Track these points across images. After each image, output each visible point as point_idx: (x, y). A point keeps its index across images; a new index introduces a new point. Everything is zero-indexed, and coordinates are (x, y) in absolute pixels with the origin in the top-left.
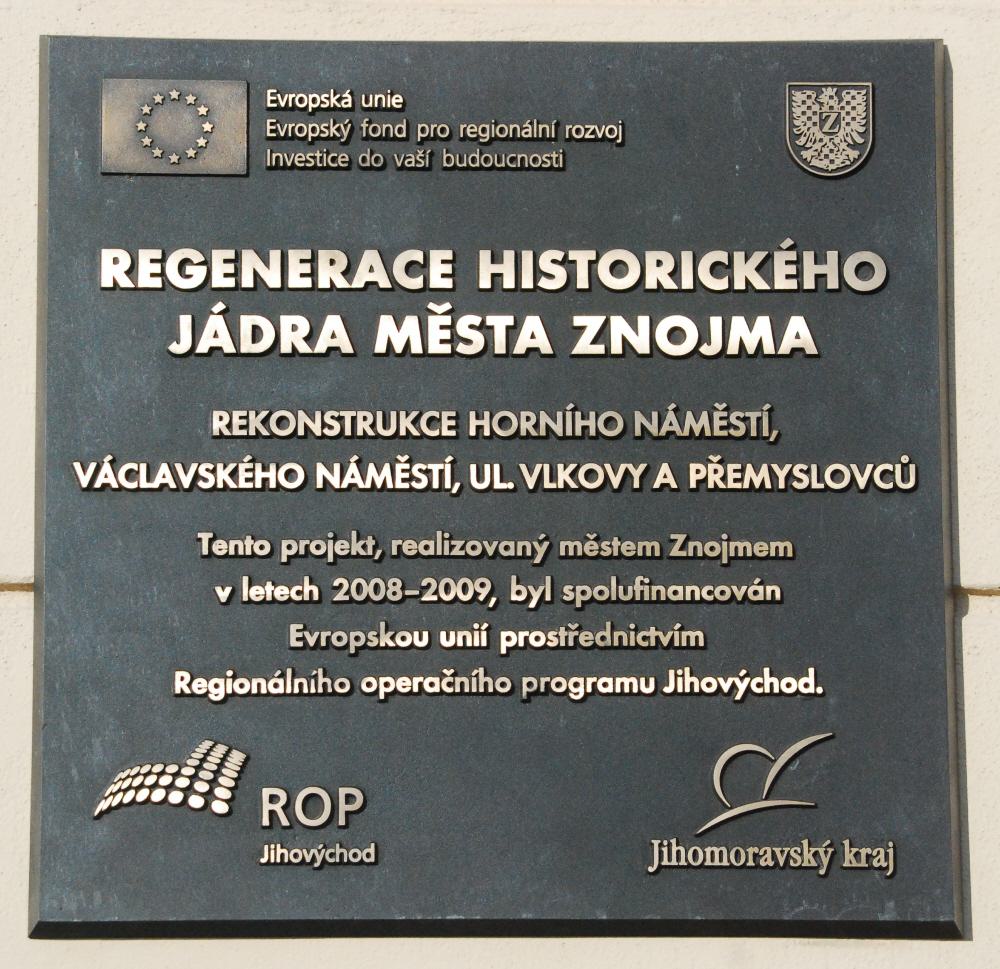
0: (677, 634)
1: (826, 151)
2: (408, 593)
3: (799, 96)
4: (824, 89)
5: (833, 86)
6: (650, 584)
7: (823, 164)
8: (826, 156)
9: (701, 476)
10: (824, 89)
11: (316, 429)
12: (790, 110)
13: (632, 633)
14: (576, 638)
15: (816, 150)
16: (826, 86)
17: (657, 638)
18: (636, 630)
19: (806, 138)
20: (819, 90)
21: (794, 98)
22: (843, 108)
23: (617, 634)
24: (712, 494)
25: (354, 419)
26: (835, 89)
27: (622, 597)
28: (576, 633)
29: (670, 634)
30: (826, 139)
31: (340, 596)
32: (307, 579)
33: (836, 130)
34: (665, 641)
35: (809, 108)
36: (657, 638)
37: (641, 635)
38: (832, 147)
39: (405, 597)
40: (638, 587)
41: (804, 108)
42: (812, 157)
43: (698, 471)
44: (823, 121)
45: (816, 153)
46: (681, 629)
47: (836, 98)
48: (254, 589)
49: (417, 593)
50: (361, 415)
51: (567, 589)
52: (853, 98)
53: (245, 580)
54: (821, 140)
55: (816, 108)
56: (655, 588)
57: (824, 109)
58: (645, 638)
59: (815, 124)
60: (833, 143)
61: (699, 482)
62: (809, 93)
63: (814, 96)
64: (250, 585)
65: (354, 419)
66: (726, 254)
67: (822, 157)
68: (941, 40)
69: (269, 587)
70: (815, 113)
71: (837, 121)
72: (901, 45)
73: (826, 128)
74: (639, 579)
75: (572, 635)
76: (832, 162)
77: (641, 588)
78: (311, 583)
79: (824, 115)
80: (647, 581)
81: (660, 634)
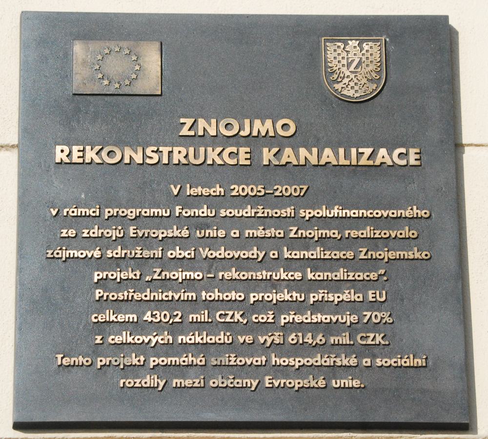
0: (182, 294)
1: (352, 84)
2: (267, 192)
3: (331, 47)
4: (349, 42)
5: (356, 40)
6: (342, 209)
7: (351, 93)
8: (352, 88)
9: (101, 295)
10: (349, 42)
11: (138, 159)
12: (354, 39)
13: (160, 294)
14: (133, 296)
15: (345, 84)
16: (351, 40)
17: (173, 296)
18: (162, 292)
19: (337, 76)
20: (346, 43)
21: (328, 48)
22: (363, 54)
23: (152, 294)
24: (247, 239)
25: (170, 152)
26: (358, 42)
27: (328, 215)
28: (133, 294)
29: (179, 294)
30: (352, 76)
31: (234, 193)
32: (218, 186)
33: (359, 70)
34: (176, 297)
35: (339, 54)
36: (173, 296)
37: (165, 294)
38: (356, 81)
39: (265, 194)
40: (336, 211)
41: (335, 54)
42: (342, 88)
43: (100, 293)
44: (349, 65)
45: (345, 86)
46: (184, 292)
47: (358, 48)
48: (192, 189)
49: (272, 192)
50: (176, 150)
51: (301, 211)
52: (371, 47)
53: (188, 186)
54: (348, 77)
55: (344, 54)
56: (344, 211)
57: (350, 56)
58: (166, 296)
59: (343, 65)
60: (357, 79)
61: (100, 297)
62: (339, 44)
63: (342, 47)
64: (190, 188)
65: (170, 152)
66: (249, 149)
67: (349, 89)
68: (446, 18)
69: (200, 189)
70: (343, 58)
71: (360, 63)
72: (20, 189)
73: (352, 69)
74: (336, 207)
75: (131, 295)
76: (356, 91)
77: (338, 211)
78: (220, 187)
79: (350, 60)
80: (341, 208)
81: (174, 294)
